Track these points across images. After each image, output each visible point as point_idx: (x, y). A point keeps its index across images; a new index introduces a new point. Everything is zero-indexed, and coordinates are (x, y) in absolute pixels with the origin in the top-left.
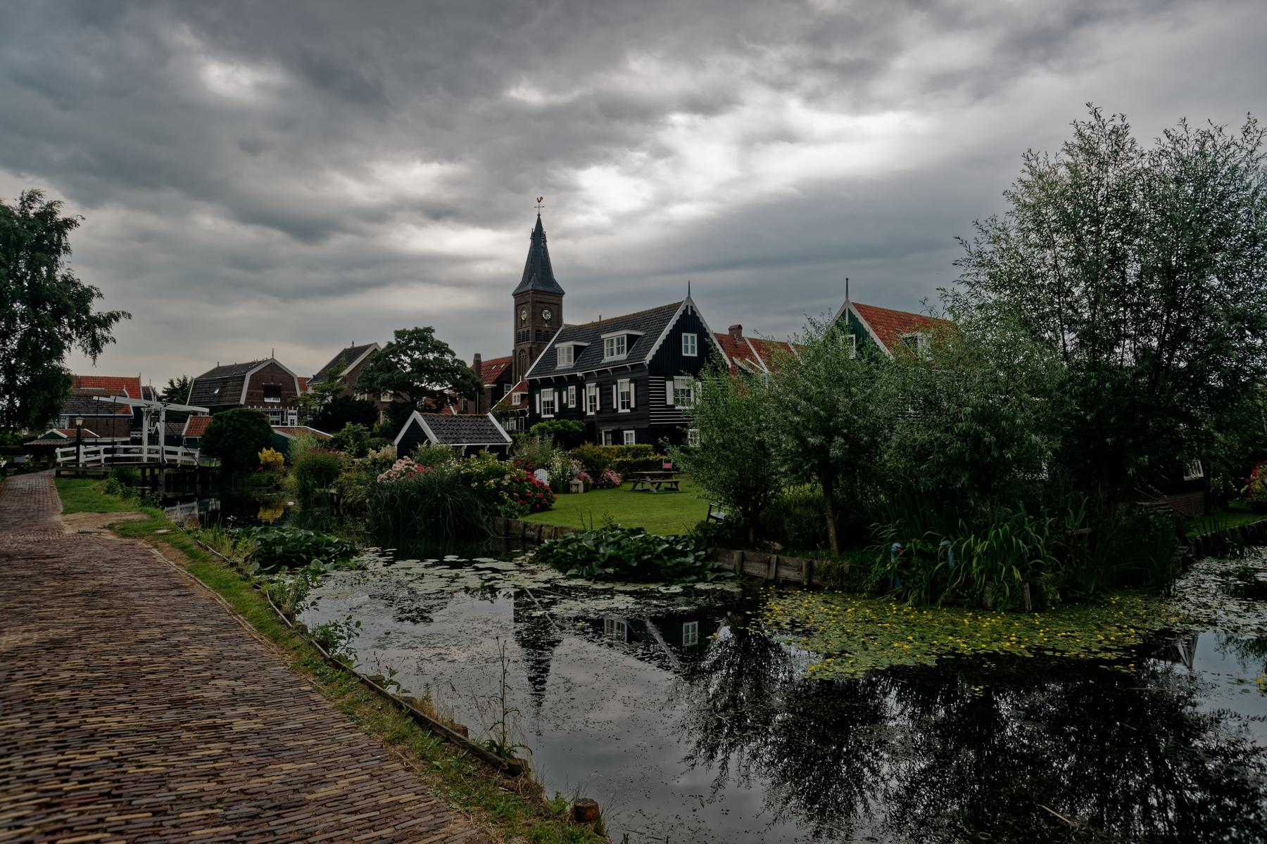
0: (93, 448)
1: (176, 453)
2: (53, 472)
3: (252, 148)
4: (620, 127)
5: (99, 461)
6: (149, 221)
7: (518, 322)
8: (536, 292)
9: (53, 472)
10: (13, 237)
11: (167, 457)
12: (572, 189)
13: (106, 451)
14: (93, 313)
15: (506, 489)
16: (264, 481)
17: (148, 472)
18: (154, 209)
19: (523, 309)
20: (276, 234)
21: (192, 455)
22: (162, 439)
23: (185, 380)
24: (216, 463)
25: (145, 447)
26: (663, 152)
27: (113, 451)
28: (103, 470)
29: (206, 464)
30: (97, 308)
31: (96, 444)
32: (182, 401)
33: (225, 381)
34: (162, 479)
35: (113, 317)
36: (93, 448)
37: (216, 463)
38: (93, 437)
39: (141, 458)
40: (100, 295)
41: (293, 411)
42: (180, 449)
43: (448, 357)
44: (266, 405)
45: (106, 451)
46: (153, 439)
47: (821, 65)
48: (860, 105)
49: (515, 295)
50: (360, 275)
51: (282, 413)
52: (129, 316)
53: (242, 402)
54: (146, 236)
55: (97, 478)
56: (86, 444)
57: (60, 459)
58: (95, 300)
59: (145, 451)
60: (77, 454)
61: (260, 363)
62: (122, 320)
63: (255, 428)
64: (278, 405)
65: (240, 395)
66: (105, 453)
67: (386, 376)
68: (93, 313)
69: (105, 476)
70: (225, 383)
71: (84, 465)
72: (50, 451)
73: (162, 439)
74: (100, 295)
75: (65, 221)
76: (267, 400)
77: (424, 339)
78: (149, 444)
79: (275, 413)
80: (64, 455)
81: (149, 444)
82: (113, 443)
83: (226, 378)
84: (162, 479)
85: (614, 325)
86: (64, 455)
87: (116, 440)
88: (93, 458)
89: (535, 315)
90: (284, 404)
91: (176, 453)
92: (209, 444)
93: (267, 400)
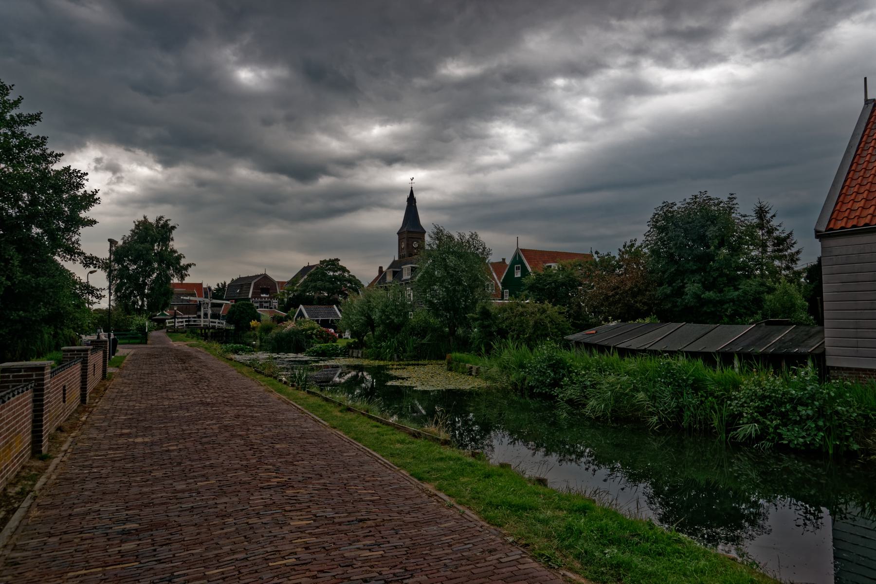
0: (181, 320)
1: (215, 322)
2: (165, 330)
3: (267, 122)
4: (516, 90)
5: (183, 326)
6: (207, 174)
7: (400, 249)
8: (409, 232)
9: (165, 330)
10: (155, 238)
11: (211, 324)
12: (483, 137)
13: (186, 321)
14: (181, 264)
15: (314, 334)
16: (252, 335)
17: (203, 331)
18: (210, 167)
19: (403, 241)
20: (284, 178)
21: (222, 323)
22: (209, 316)
23: (225, 283)
24: (232, 327)
25: (202, 319)
26: (547, 107)
27: (189, 321)
28: (185, 329)
29: (227, 328)
30: (183, 262)
31: (182, 318)
32: (221, 298)
33: (242, 286)
34: (209, 334)
35: (189, 265)
36: (181, 320)
37: (232, 327)
38: (180, 315)
39: (200, 325)
40: (184, 257)
41: (275, 301)
42: (217, 321)
43: (346, 274)
44: (262, 298)
45: (186, 321)
46: (206, 315)
47: (670, 33)
48: (697, 63)
49: (398, 233)
50: (339, 204)
51: (270, 302)
52: (195, 265)
53: (250, 296)
54: (202, 183)
55: (182, 333)
56: (178, 318)
57: (168, 325)
58: (182, 259)
59: (202, 321)
60: (175, 323)
61: (258, 276)
62: (192, 266)
63: (249, 311)
64: (268, 298)
65: (249, 293)
66: (24, 382)
67: (313, 284)
68: (181, 264)
69: (185, 332)
70: (242, 286)
71: (177, 327)
72: (163, 321)
73: (209, 316)
74: (184, 257)
75: (172, 227)
76: (262, 296)
77: (333, 265)
78: (204, 318)
79: (266, 302)
80: (169, 323)
81: (204, 318)
82: (189, 318)
83: (241, 283)
84: (209, 334)
85: (23, 368)
86: (169, 323)
87: (190, 316)
88: (181, 324)
89: (409, 245)
90: (270, 298)
91: (215, 322)
92: (230, 318)
93: (262, 296)
